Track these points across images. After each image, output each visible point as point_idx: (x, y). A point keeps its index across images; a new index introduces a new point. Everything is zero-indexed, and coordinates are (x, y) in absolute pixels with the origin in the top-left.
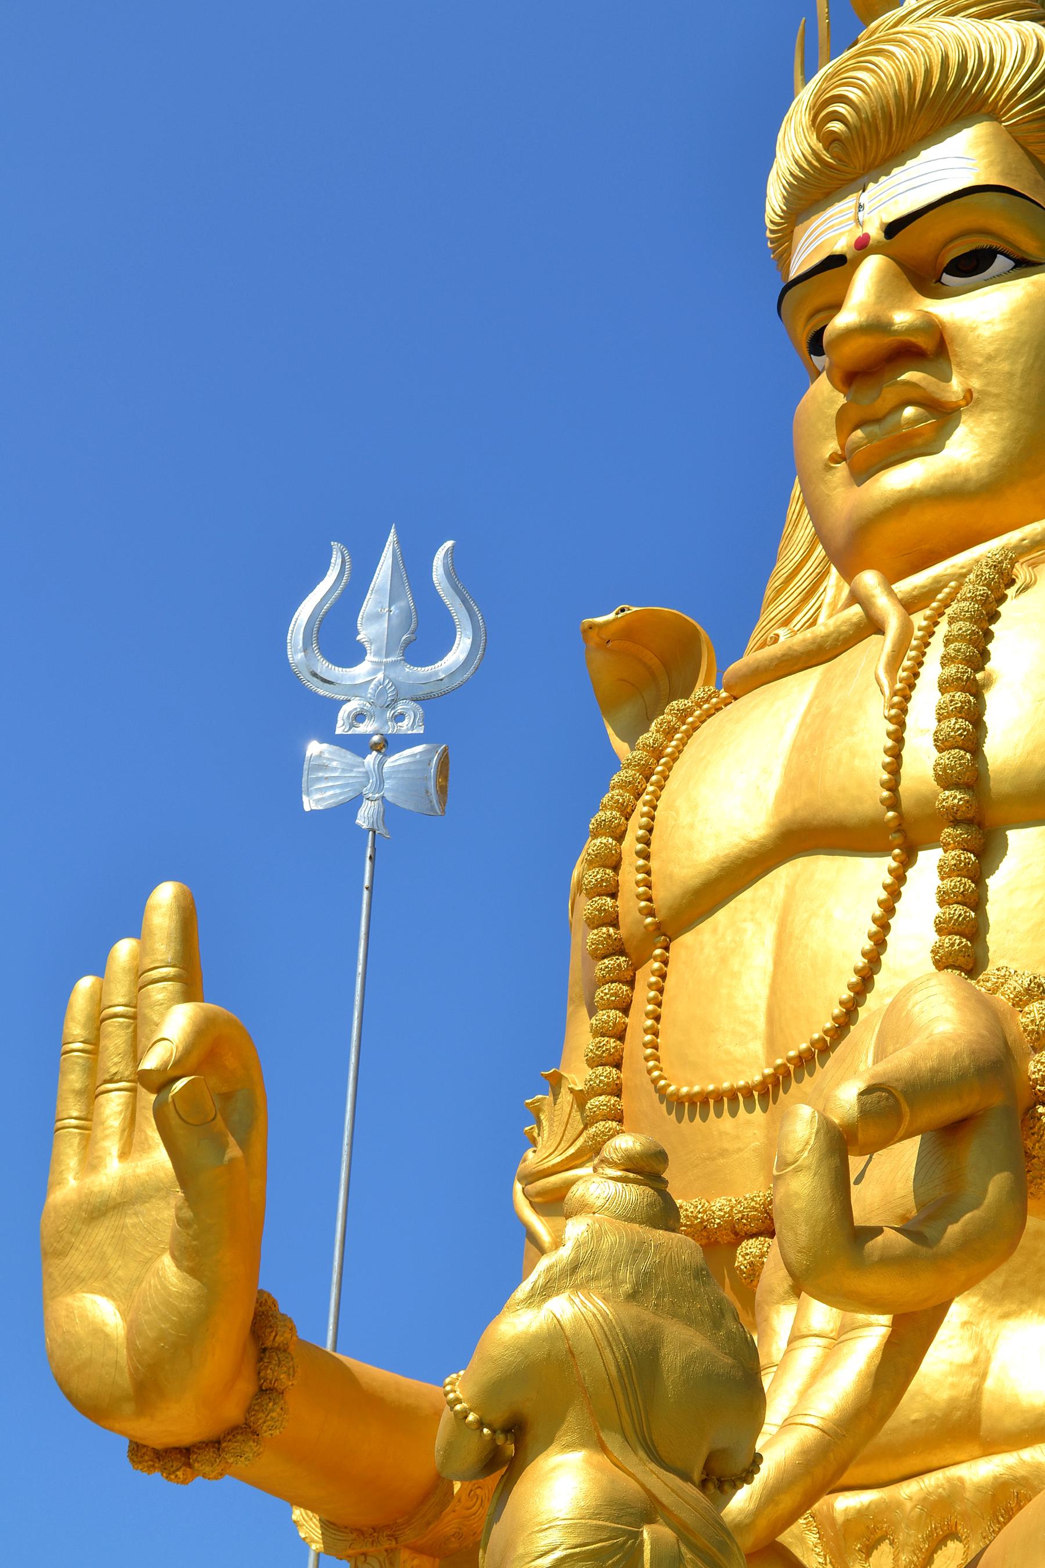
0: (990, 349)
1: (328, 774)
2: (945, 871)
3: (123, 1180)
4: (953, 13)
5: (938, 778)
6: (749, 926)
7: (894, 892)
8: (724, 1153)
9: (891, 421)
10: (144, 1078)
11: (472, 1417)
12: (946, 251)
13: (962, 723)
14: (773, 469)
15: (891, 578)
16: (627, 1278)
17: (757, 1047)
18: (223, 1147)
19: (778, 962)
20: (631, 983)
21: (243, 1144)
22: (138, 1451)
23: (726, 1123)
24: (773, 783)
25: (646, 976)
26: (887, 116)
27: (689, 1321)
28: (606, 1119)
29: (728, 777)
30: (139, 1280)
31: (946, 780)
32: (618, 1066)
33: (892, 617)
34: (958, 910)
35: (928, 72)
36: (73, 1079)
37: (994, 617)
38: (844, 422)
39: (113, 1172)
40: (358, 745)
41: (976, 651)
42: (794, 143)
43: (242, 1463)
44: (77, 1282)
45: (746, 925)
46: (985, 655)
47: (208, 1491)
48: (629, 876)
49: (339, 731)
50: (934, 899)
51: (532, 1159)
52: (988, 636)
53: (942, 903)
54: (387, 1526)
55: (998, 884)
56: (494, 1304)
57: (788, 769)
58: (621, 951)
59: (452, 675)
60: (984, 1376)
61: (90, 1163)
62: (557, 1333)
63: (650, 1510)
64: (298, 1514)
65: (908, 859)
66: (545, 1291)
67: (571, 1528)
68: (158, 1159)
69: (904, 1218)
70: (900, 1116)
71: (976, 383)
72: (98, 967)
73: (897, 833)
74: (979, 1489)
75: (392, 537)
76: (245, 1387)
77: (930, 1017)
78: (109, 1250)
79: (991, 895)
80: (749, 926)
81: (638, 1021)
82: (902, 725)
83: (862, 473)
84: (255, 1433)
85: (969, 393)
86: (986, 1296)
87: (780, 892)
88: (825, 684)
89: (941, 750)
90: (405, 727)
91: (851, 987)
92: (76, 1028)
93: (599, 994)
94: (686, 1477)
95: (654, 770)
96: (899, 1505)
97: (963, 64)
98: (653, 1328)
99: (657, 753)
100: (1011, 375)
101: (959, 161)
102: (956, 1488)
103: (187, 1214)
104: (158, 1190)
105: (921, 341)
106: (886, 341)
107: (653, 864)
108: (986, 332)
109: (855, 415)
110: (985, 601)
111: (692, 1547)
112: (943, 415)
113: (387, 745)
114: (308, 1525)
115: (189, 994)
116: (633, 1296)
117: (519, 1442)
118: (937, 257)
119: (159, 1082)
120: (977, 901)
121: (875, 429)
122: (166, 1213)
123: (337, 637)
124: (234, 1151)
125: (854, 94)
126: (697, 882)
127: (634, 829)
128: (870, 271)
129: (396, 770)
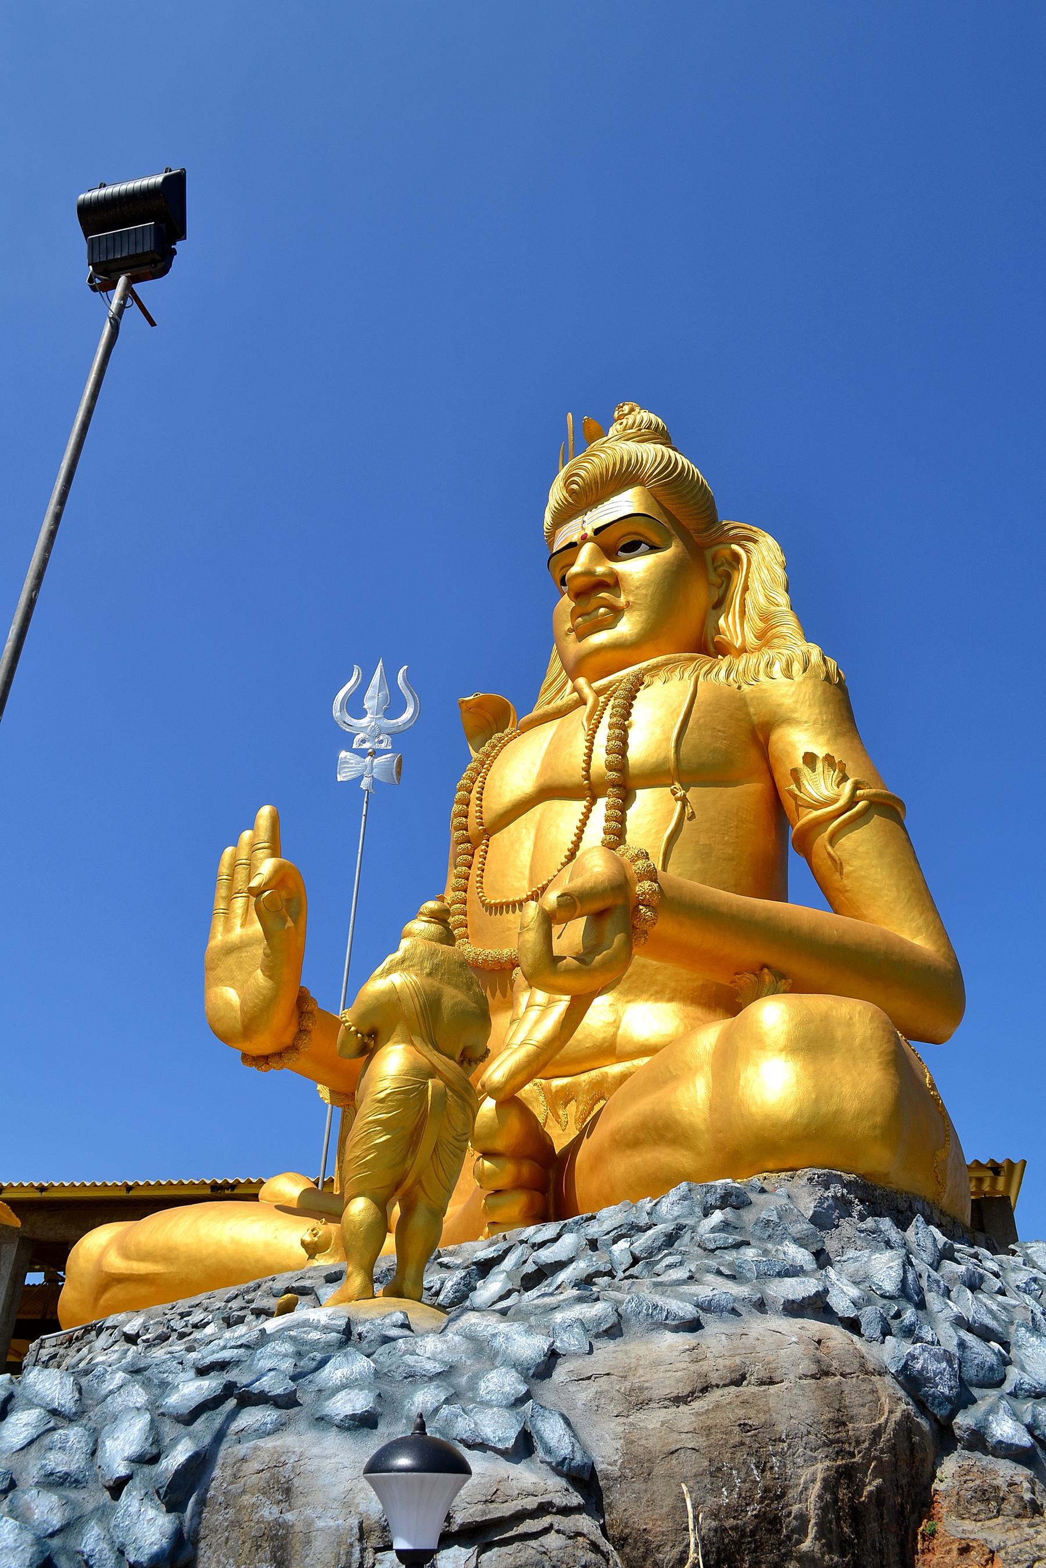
0: (637, 584)
1: (349, 766)
2: (608, 807)
4: (627, 440)
5: (606, 766)
6: (524, 831)
7: (586, 816)
9: (594, 614)
10: (250, 890)
11: (353, 1029)
12: (620, 542)
13: (618, 743)
14: (545, 639)
16: (428, 966)
17: (525, 883)
18: (285, 922)
19: (535, 846)
20: (472, 855)
21: (295, 921)
22: (245, 1057)
23: (510, 916)
24: (536, 769)
25: (479, 852)
26: (596, 482)
27: (456, 986)
29: (519, 765)
30: (247, 981)
31: (610, 767)
32: (465, 891)
33: (590, 699)
34: (614, 824)
35: (614, 464)
36: (222, 892)
37: (634, 698)
38: (574, 614)
39: (238, 932)
40: (362, 753)
41: (625, 712)
42: (557, 493)
43: (291, 1063)
44: (220, 981)
45: (523, 829)
46: (629, 714)
47: (277, 1075)
48: (473, 808)
49: (354, 746)
50: (603, 819)
52: (631, 706)
53: (606, 821)
55: (632, 814)
56: (365, 978)
57: (543, 762)
60: (618, 1028)
61: (228, 929)
62: (393, 990)
64: (319, 1087)
65: (593, 802)
66: (389, 971)
67: (395, 1079)
68: (257, 928)
69: (577, 953)
70: (576, 907)
71: (631, 599)
72: (235, 843)
73: (587, 790)
74: (614, 1077)
75: (380, 664)
76: (293, 1029)
77: (596, 865)
79: (628, 818)
80: (524, 831)
81: (474, 872)
82: (592, 743)
83: (581, 637)
86: (621, 993)
87: (538, 815)
88: (561, 726)
89: (608, 754)
90: (383, 746)
91: (566, 857)
92: (224, 869)
94: (451, 1058)
95: (486, 763)
96: (580, 1084)
98: (438, 989)
99: (488, 755)
100: (646, 595)
101: (627, 502)
102: (605, 1076)
103: (268, 951)
105: (608, 580)
106: (593, 579)
107: (484, 803)
108: (636, 576)
109: (579, 611)
110: (630, 691)
111: (452, 1090)
112: (617, 612)
113: (375, 754)
114: (324, 1092)
115: (273, 855)
116: (430, 974)
117: (374, 1039)
119: (256, 893)
120: (622, 820)
121: (587, 617)
122: (259, 951)
124: (290, 923)
125: (582, 473)
126: (502, 811)
127: (476, 788)
128: (587, 549)
129: (378, 764)
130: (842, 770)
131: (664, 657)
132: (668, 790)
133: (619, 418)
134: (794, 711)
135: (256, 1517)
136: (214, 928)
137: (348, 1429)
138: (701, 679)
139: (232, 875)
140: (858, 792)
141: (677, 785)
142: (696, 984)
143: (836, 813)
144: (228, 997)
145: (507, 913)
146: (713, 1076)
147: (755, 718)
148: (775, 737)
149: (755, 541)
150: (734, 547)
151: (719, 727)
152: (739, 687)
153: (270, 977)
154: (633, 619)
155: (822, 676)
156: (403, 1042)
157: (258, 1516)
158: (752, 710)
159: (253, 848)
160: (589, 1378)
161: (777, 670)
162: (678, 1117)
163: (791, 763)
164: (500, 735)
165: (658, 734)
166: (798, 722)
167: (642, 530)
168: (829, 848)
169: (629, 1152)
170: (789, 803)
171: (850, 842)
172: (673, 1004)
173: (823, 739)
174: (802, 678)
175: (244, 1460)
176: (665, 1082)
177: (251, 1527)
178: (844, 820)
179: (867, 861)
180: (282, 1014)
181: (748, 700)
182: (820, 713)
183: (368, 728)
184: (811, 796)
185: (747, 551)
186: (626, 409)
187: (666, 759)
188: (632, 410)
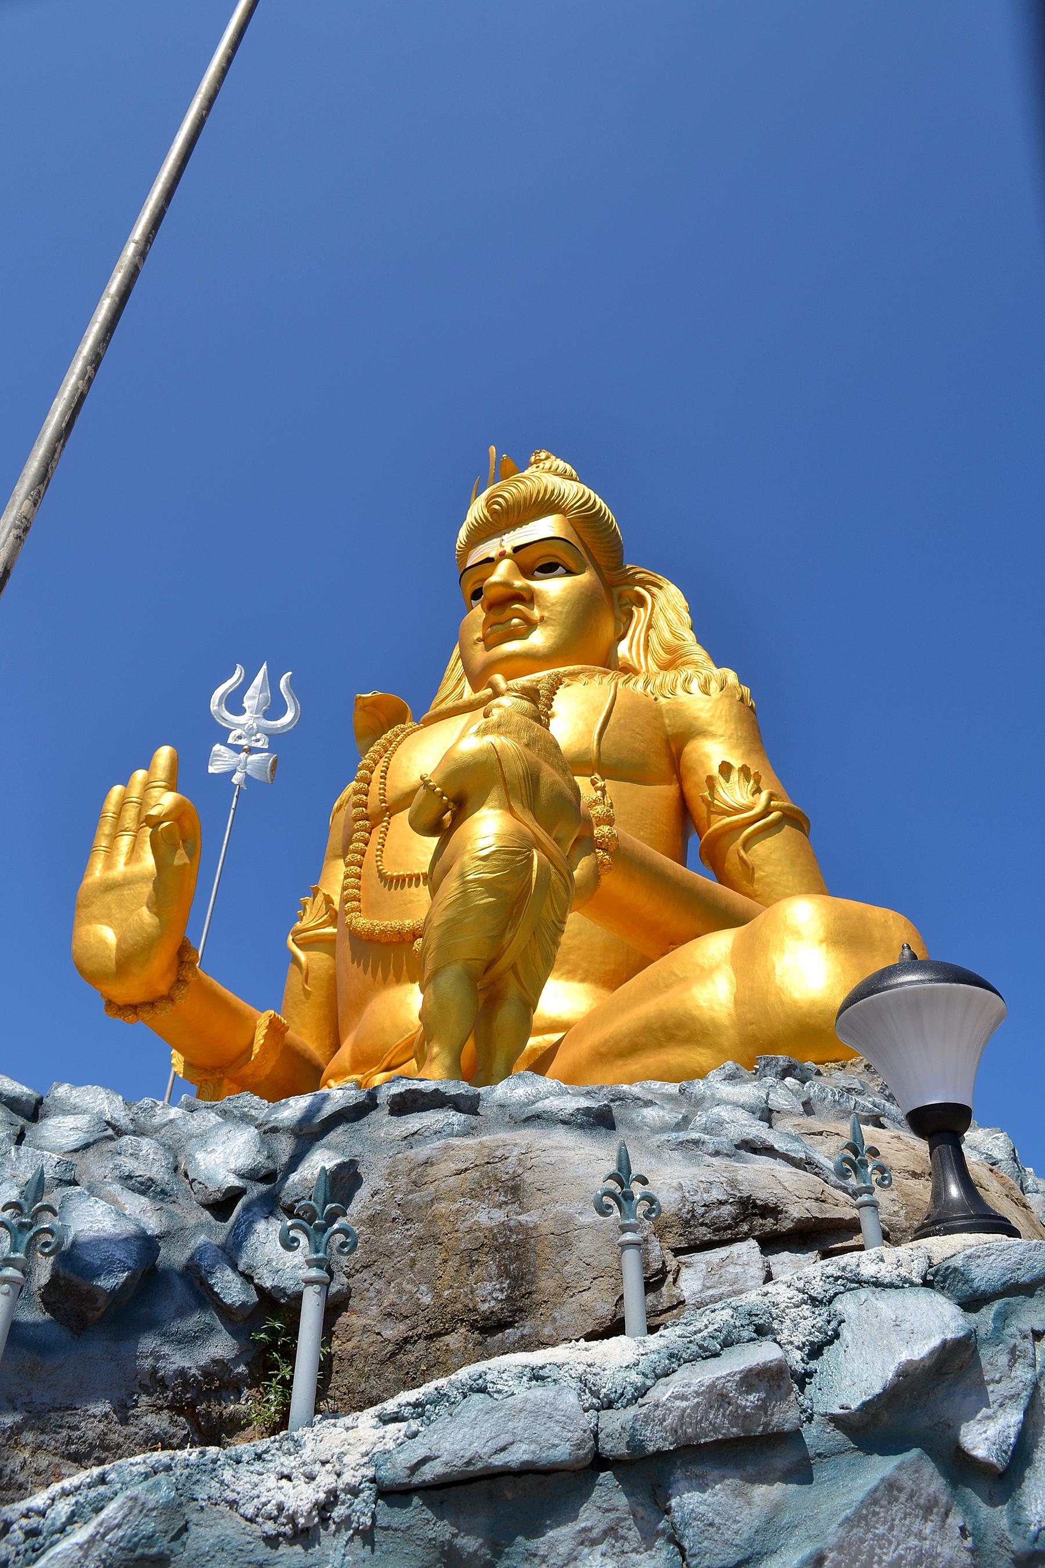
0: (554, 601)
3: (125, 874)
8: (411, 902)
9: (506, 625)
12: (540, 562)
15: (508, 678)
22: (110, 1003)
28: (353, 888)
35: (539, 492)
36: (106, 829)
39: (120, 868)
40: (237, 749)
42: (477, 510)
44: (97, 919)
48: (375, 788)
49: (230, 741)
51: (299, 925)
54: (220, 1067)
58: (366, 818)
59: (283, 727)
61: (109, 865)
63: (538, 844)
68: (148, 861)
71: (546, 614)
72: (125, 781)
75: (265, 666)
76: (171, 978)
78: (113, 906)
83: (488, 648)
84: (184, 981)
85: (542, 619)
90: (259, 745)
93: (355, 835)
97: (553, 491)
100: (561, 612)
104: (143, 879)
106: (511, 591)
107: (388, 782)
112: (530, 625)
113: (251, 751)
116: (527, 745)
118: (534, 563)
123: (234, 703)
125: (506, 495)
126: (409, 789)
127: (380, 767)
129: (253, 762)
130: (757, 782)
131: (580, 666)
132: (588, 779)
133: (536, 462)
134: (710, 724)
135: (463, 1227)
136: (92, 865)
137: (581, 1126)
138: (620, 686)
139: (119, 814)
140: (772, 803)
141: (597, 776)
142: (608, 968)
143: (751, 820)
144: (103, 936)
145: (410, 886)
146: (736, 971)
147: (669, 729)
148: (688, 749)
149: (660, 588)
150: (638, 589)
151: (637, 730)
152: (656, 699)
153: (157, 914)
154: (547, 633)
155: (738, 697)
156: (500, 808)
157: (468, 1224)
158: (667, 721)
159: (147, 786)
160: (821, 1133)
161: (694, 686)
162: (695, 1013)
163: (705, 772)
164: (402, 726)
165: (581, 726)
166: (713, 735)
167: (560, 554)
168: (742, 853)
169: (620, 1063)
170: (700, 810)
171: (763, 849)
172: (585, 985)
173: (737, 753)
174: (718, 696)
175: (428, 1163)
176: (667, 987)
177: (458, 1239)
178: (759, 827)
179: (779, 869)
180: (161, 960)
181: (664, 711)
182: (736, 729)
183: (248, 724)
184: (725, 803)
185: (653, 595)
186: (543, 455)
187: (587, 751)
188: (547, 458)
